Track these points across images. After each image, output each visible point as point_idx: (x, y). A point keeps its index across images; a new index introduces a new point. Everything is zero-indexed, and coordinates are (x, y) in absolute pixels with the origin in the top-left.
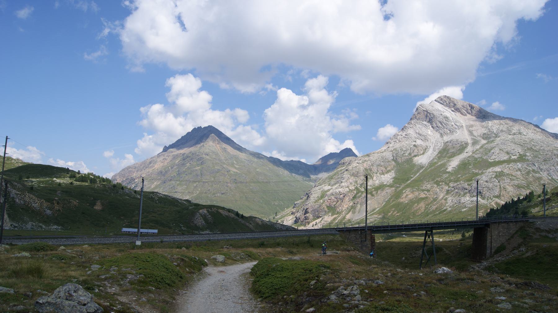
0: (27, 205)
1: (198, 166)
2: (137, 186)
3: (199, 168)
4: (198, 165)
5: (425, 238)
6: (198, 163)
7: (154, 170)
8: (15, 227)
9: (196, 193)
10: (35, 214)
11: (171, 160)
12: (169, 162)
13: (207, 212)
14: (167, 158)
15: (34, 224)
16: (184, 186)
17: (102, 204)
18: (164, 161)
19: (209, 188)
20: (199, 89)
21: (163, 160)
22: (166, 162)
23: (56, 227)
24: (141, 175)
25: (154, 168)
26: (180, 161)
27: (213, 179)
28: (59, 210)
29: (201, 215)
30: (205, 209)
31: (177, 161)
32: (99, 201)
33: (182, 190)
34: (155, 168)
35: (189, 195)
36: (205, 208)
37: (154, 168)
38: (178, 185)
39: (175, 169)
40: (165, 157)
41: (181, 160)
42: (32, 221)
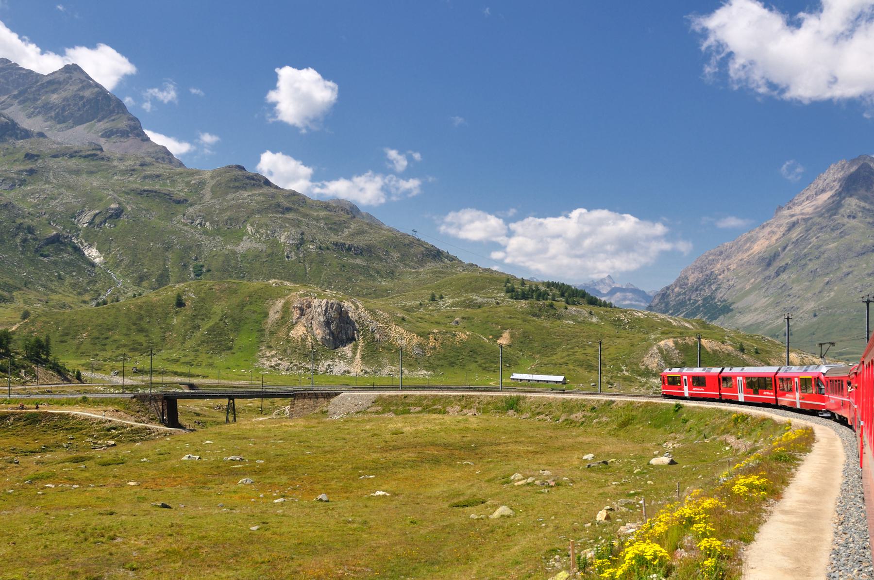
0: (391, 343)
1: (834, 242)
2: (720, 288)
3: (835, 244)
4: (834, 240)
5: (799, 409)
6: (834, 235)
7: (750, 255)
8: (366, 372)
9: (829, 296)
10: (400, 355)
11: (784, 234)
12: (780, 238)
13: (673, 345)
14: (776, 229)
15: (393, 368)
16: (806, 283)
17: (512, 336)
18: (771, 237)
19: (857, 284)
20: (271, 186)
21: (769, 234)
22: (774, 238)
23: (424, 372)
24: (728, 265)
25: (752, 251)
26: (799, 234)
27: (865, 265)
28: (435, 348)
29: (661, 350)
30: (671, 340)
31: (795, 235)
32: (508, 331)
33: (801, 292)
34: (755, 251)
35: (815, 301)
36: (671, 337)
37: (752, 251)
38: (793, 282)
39: (790, 250)
40: (772, 229)
41: (801, 233)
42: (392, 365)
